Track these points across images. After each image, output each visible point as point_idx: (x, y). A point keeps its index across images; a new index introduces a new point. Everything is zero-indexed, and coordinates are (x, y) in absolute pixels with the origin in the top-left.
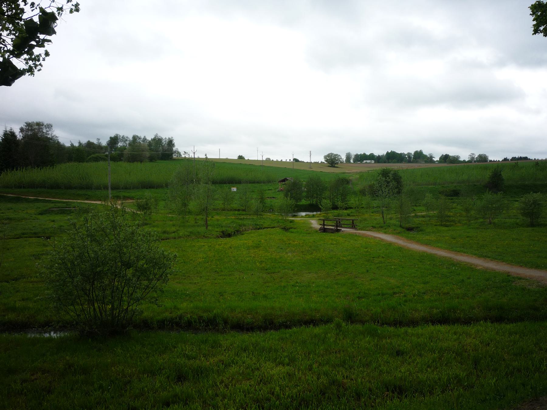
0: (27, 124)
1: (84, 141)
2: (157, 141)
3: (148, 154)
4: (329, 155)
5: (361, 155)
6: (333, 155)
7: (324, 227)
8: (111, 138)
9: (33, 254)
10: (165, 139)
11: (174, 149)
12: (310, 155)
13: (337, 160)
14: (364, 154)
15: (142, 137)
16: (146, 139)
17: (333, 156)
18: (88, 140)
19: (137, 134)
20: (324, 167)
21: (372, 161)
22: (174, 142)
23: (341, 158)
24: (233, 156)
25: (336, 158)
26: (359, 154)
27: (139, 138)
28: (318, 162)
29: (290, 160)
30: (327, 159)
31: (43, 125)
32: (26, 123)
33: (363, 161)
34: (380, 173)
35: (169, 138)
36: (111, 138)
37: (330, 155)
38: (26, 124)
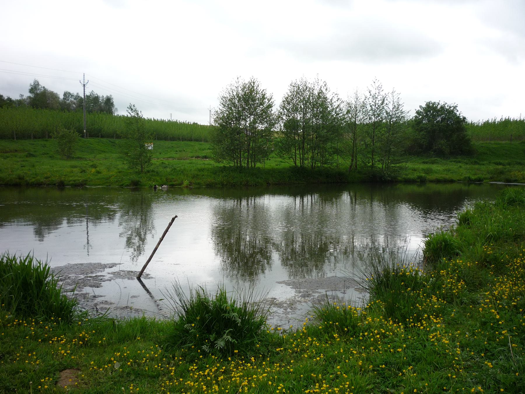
16: (79, 97)
19: (69, 91)
27: (72, 96)
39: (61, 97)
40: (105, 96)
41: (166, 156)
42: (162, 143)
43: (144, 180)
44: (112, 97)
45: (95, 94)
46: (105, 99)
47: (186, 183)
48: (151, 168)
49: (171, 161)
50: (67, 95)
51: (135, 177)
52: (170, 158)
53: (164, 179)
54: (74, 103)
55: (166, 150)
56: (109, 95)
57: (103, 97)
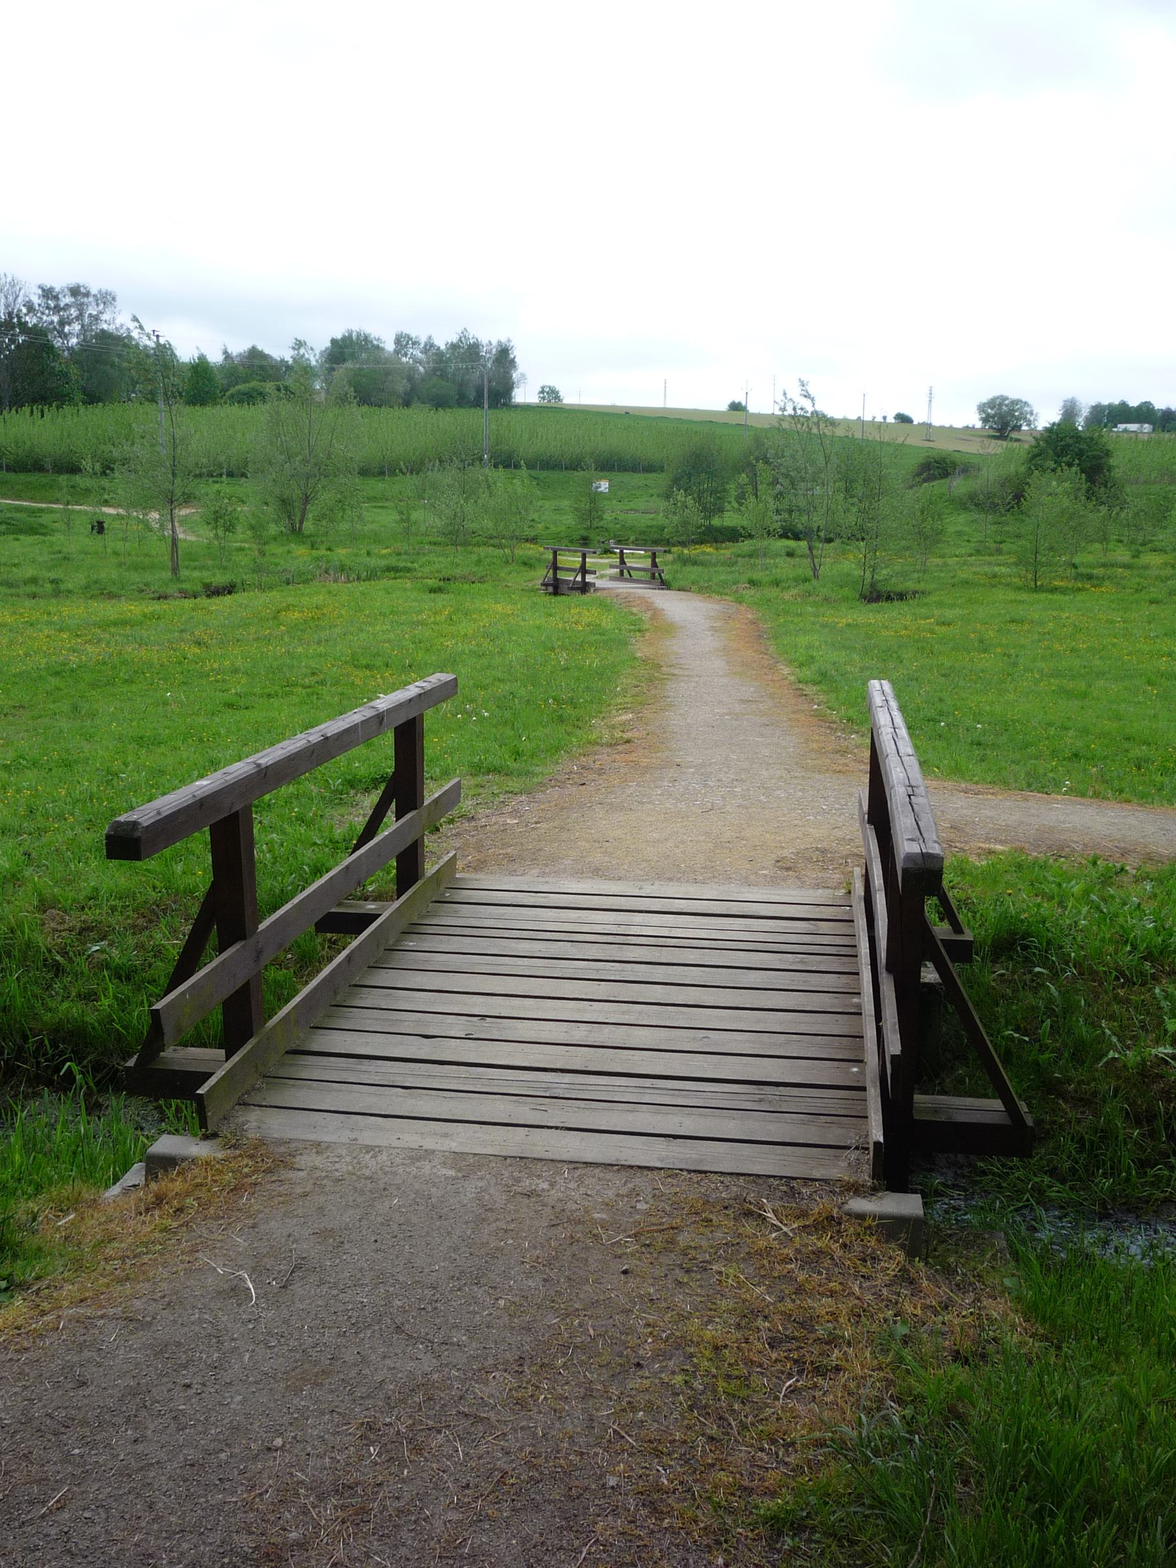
0: (43, 290)
1: (238, 348)
2: (468, 351)
3: (402, 386)
4: (992, 403)
5: (1110, 406)
6: (1007, 402)
7: (583, 577)
8: (334, 341)
9: (1095, 854)
10: (487, 345)
11: (514, 375)
12: (930, 401)
13: (1018, 419)
14: (1123, 404)
15: (423, 340)
16: (432, 345)
17: (1006, 406)
18: (250, 346)
19: (406, 331)
20: (973, 438)
21: (1146, 426)
22: (515, 353)
23: (1032, 414)
24: (718, 403)
25: (1015, 411)
26: (1106, 403)
27: (414, 343)
28: (973, 427)
29: (885, 418)
30: (988, 415)
31: (87, 295)
32: (39, 287)
33: (1116, 427)
34: (1039, 436)
35: (500, 343)
36: (334, 341)
37: (998, 401)
38: (40, 292)
39: (390, 346)
40: (494, 343)
41: (625, 508)
42: (626, 477)
43: (592, 535)
44: (512, 344)
45: (471, 337)
46: (494, 350)
47: (632, 538)
48: (601, 524)
49: (631, 516)
50: (403, 341)
51: (584, 533)
52: (631, 510)
53: (612, 535)
54: (420, 362)
55: (634, 492)
56: (504, 340)
57: (491, 344)
